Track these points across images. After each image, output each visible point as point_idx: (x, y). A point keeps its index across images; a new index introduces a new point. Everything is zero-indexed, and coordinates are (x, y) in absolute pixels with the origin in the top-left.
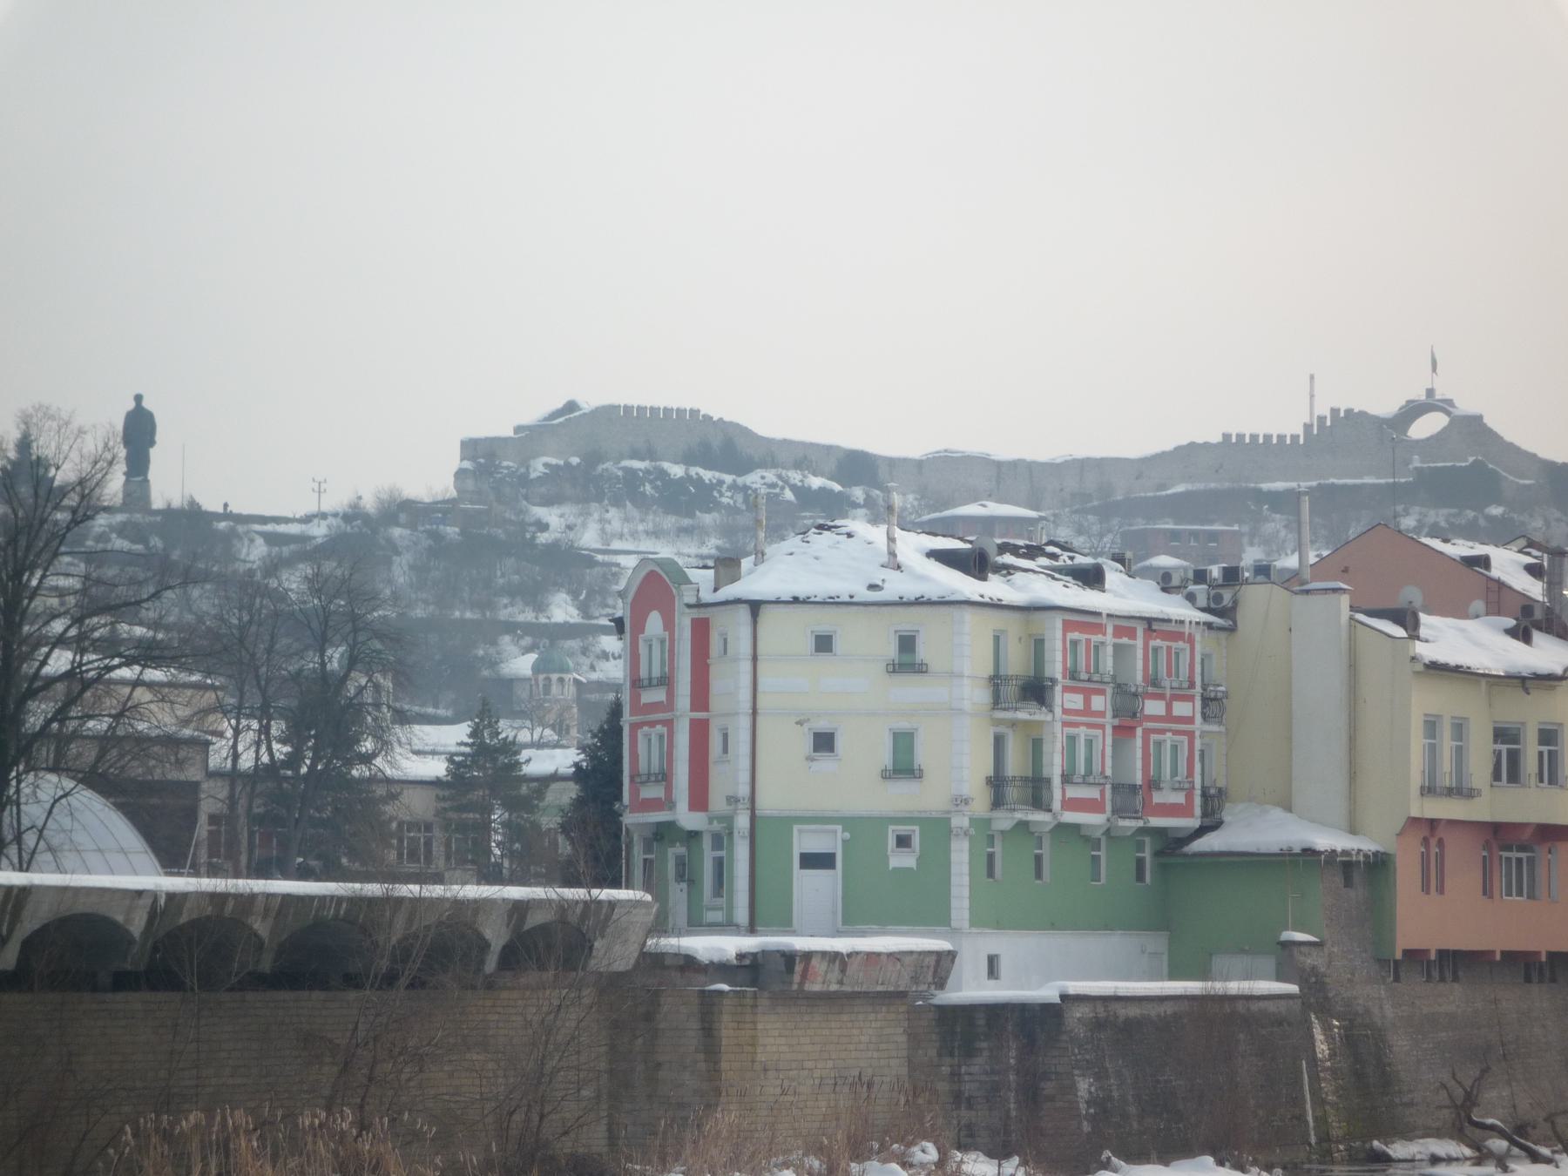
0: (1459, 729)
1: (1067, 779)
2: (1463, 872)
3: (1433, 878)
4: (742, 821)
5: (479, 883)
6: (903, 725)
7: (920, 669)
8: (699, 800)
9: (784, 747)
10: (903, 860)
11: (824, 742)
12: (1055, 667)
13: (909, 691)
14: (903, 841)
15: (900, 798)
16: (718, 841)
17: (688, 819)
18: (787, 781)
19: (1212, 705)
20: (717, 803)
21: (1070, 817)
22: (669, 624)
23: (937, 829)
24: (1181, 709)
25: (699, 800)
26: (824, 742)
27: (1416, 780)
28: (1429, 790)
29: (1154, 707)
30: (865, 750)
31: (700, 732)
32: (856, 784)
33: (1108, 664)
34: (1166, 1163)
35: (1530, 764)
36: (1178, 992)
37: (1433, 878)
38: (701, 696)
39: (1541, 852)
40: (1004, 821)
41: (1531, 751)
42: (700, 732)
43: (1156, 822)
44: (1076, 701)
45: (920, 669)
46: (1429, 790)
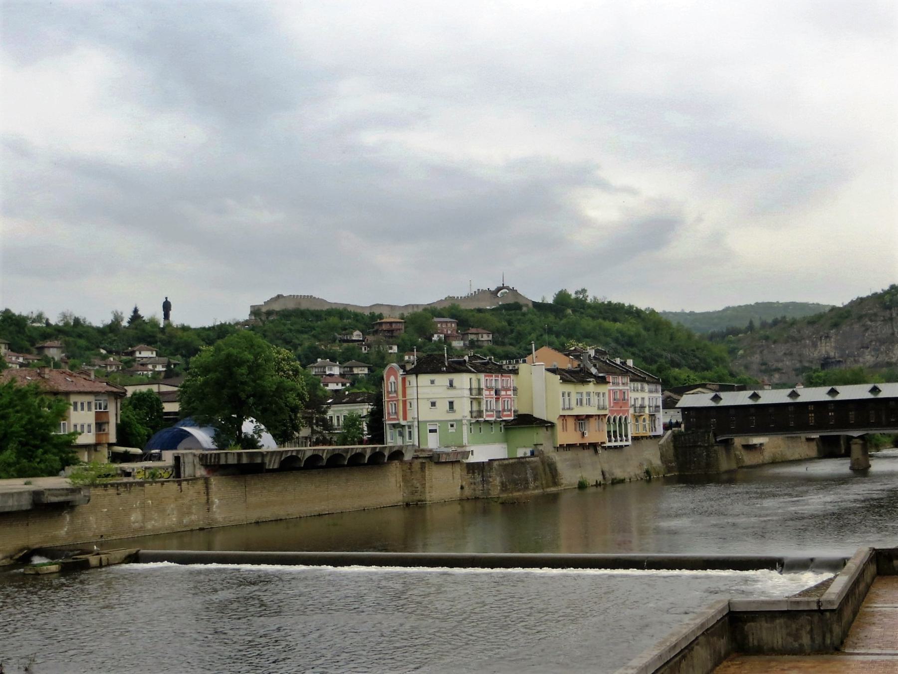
0: (569, 395)
1: (487, 410)
2: (571, 423)
3: (565, 428)
4: (416, 423)
5: (117, 425)
6: (451, 400)
7: (455, 388)
8: (405, 418)
9: (425, 406)
10: (452, 430)
11: (433, 404)
12: (483, 386)
13: (452, 393)
14: (452, 426)
15: (451, 417)
16: (409, 427)
17: (403, 423)
18: (425, 413)
19: (515, 390)
20: (409, 418)
21: (487, 419)
22: (396, 378)
23: (460, 422)
24: (509, 393)
25: (405, 418)
26: (433, 404)
27: (561, 406)
28: (564, 409)
29: (503, 393)
30: (443, 406)
31: (404, 402)
32: (441, 413)
33: (493, 384)
34: (818, 304)
35: (584, 402)
36: (58, 487)
37: (565, 428)
38: (404, 395)
39: (586, 421)
40: (474, 421)
41: (585, 398)
42: (404, 402)
43: (505, 418)
44: (487, 393)
45: (455, 388)
46: (564, 409)
